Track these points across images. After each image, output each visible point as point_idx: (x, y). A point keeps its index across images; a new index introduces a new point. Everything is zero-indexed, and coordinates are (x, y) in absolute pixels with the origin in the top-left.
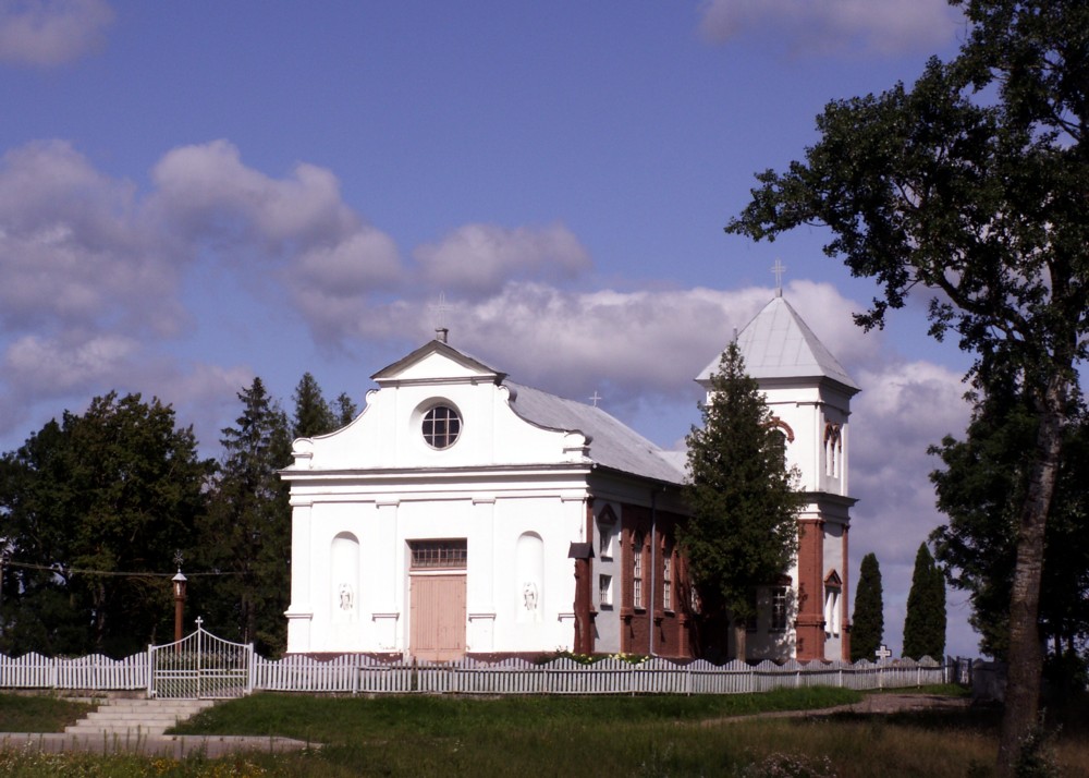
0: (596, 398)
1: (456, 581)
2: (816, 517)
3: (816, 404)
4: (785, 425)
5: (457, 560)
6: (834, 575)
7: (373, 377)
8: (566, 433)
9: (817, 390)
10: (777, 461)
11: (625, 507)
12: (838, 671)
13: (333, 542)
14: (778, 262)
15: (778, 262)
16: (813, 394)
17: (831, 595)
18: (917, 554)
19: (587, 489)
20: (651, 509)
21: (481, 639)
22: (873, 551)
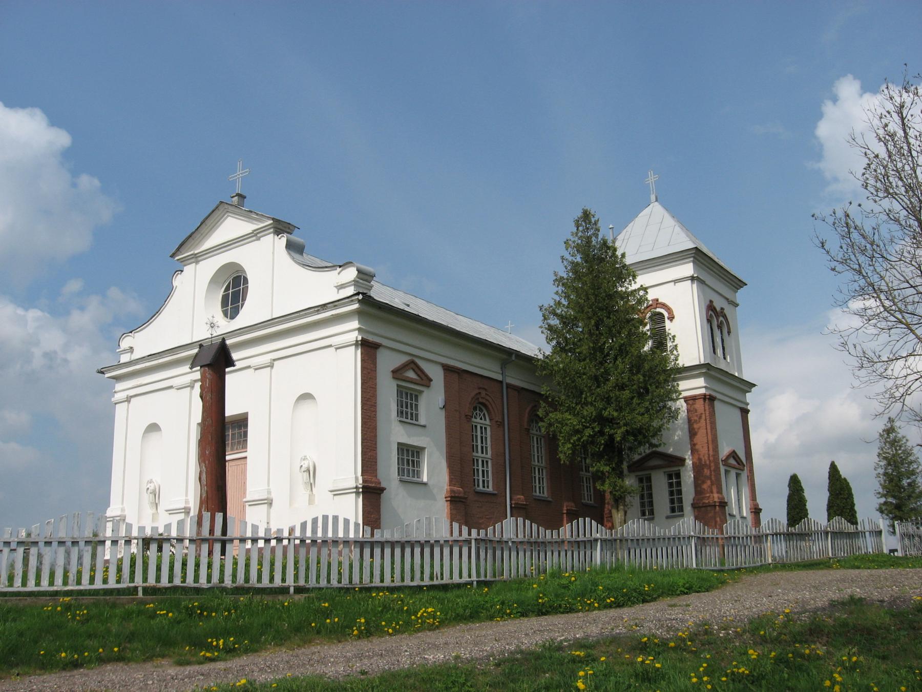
0: (509, 327)
1: (242, 462)
2: (703, 391)
3: (692, 278)
4: (664, 306)
5: (239, 443)
6: (733, 455)
7: (173, 256)
8: (339, 269)
9: (691, 265)
10: (661, 339)
11: (447, 369)
12: (269, 486)
13: (143, 436)
14: (651, 174)
15: (651, 174)
16: (688, 269)
17: (733, 473)
18: (828, 470)
19: (359, 330)
20: (501, 382)
21: (247, 536)
22: (792, 474)
